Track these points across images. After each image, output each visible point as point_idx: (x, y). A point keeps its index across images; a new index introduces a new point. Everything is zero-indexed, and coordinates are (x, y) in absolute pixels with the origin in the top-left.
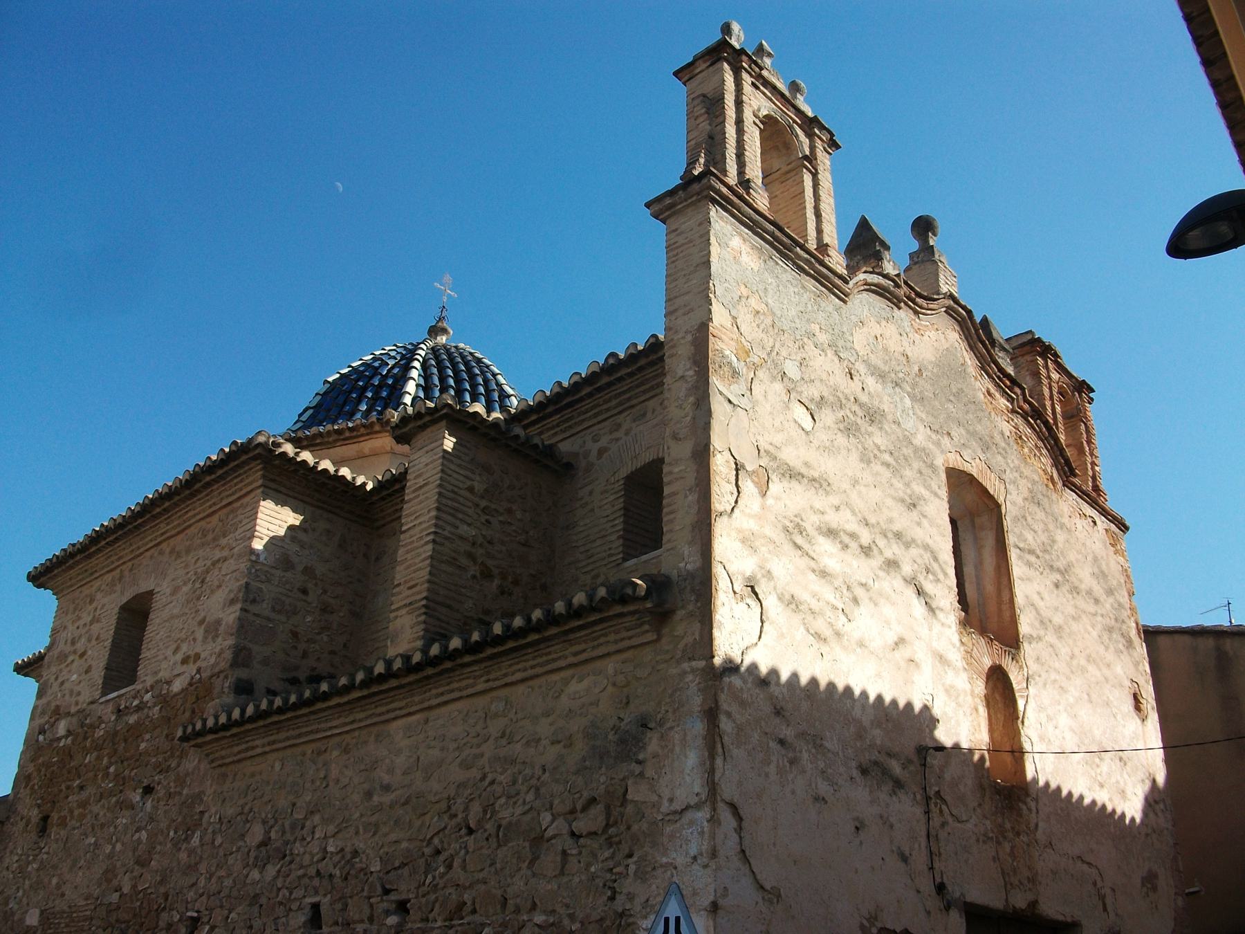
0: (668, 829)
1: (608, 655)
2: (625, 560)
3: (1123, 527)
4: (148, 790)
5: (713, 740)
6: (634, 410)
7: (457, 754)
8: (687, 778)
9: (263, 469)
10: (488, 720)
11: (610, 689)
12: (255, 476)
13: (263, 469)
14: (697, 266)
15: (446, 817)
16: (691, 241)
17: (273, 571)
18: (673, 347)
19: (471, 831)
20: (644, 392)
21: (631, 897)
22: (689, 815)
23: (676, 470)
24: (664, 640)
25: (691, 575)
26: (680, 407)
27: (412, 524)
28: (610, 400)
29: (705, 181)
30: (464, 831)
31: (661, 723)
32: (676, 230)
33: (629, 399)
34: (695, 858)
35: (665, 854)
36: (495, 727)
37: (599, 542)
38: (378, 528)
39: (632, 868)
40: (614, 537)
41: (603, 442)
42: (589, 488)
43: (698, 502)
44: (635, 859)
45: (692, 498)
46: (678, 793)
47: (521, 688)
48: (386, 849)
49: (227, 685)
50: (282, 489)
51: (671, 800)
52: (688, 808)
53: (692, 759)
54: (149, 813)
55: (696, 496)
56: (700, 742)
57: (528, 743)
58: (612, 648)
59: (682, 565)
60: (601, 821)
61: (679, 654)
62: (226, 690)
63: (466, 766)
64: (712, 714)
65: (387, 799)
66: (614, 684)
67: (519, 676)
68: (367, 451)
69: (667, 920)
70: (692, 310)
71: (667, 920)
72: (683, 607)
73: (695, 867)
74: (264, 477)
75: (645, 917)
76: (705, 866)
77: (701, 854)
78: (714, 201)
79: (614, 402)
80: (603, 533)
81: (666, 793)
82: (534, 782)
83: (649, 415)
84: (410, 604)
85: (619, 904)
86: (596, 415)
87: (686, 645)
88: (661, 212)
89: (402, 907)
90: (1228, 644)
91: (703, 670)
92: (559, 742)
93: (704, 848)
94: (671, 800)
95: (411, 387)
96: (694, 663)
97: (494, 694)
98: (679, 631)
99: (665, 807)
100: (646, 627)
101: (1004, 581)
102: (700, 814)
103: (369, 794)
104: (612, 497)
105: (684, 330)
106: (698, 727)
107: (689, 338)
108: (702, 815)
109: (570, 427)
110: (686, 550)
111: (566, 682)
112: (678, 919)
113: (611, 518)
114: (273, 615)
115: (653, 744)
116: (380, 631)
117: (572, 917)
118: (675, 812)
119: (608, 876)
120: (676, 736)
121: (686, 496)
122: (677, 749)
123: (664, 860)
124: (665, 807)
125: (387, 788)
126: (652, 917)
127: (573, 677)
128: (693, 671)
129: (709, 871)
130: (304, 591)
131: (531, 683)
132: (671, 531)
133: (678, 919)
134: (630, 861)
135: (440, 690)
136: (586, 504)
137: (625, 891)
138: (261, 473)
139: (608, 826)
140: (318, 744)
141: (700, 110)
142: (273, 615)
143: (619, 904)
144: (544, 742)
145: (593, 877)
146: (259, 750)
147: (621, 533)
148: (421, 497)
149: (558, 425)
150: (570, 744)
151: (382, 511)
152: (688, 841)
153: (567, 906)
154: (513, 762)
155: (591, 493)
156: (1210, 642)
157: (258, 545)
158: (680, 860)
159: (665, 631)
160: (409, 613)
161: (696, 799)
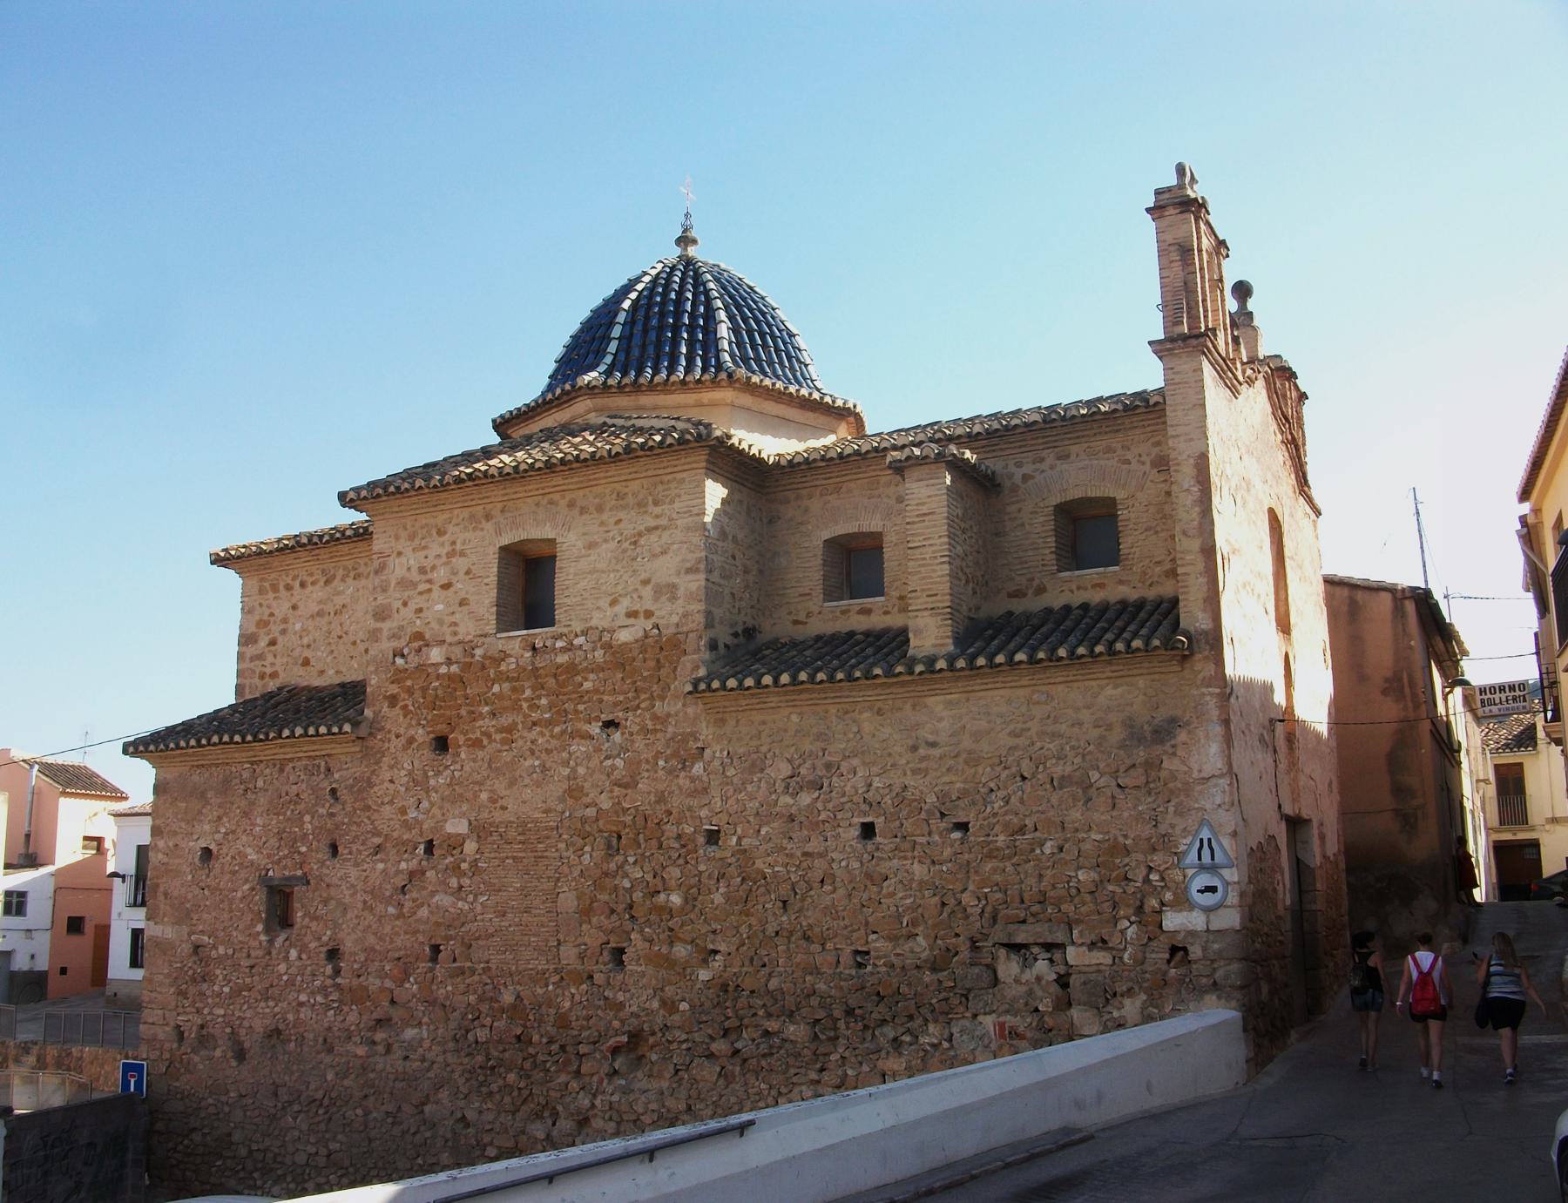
0: (1198, 788)
1: (1142, 674)
2: (1059, 571)
3: (1318, 513)
4: (610, 724)
5: (1228, 740)
6: (1056, 450)
7: (1004, 726)
8: (1211, 759)
9: (709, 454)
10: (1031, 706)
11: (1141, 697)
12: (700, 458)
13: (709, 454)
14: (1195, 405)
15: (998, 769)
16: (1186, 383)
17: (718, 543)
18: (1178, 464)
19: (1024, 778)
20: (1070, 439)
21: (1172, 826)
22: (1214, 781)
23: (1188, 558)
24: (1186, 671)
25: (1205, 633)
26: (1188, 512)
27: (920, 544)
28: (1037, 438)
29: (1202, 340)
30: (1018, 779)
31: (1188, 723)
32: (1172, 369)
33: (1056, 441)
34: (1219, 805)
35: (1197, 801)
36: (1038, 712)
37: (1030, 553)
38: (768, 493)
39: (1171, 809)
40: (1047, 551)
41: (1027, 469)
42: (1018, 506)
43: (1208, 583)
44: (1172, 803)
45: (1203, 580)
46: (1204, 767)
47: (1060, 687)
48: (940, 788)
49: (702, 643)
50: (715, 469)
51: (1200, 771)
52: (1213, 776)
53: (1214, 748)
54: (620, 745)
55: (1206, 580)
56: (1220, 738)
57: (1073, 725)
58: (1145, 671)
59: (1197, 624)
60: (1143, 779)
61: (1199, 682)
62: (703, 648)
63: (1014, 734)
64: (1226, 722)
65: (936, 752)
66: (1145, 694)
67: (1061, 679)
68: (705, 401)
69: (1201, 840)
70: (1191, 440)
71: (1201, 840)
72: (1200, 652)
73: (1220, 810)
74: (708, 461)
75: (1185, 837)
76: (1227, 810)
77: (1224, 803)
78: (1204, 353)
79: (1040, 441)
80: (1036, 546)
81: (1195, 767)
82: (1081, 750)
83: (1073, 457)
84: (932, 609)
85: (1163, 829)
86: (1020, 447)
87: (1204, 678)
88: (1161, 351)
89: (963, 827)
90: (1360, 595)
91: (1218, 694)
92: (1100, 727)
93: (1226, 800)
94: (1200, 771)
95: (724, 330)
96: (1210, 689)
97: (1036, 688)
98: (1198, 667)
99: (1195, 774)
100: (1175, 662)
101: (1282, 584)
102: (1222, 781)
103: (914, 748)
104: (1042, 519)
105: (1187, 453)
106: (1218, 729)
107: (1192, 461)
108: (1224, 782)
109: (994, 451)
110: (1200, 615)
111: (1102, 688)
112: (1209, 840)
113: (1043, 535)
114: (722, 582)
115: (1182, 736)
116: (787, 588)
117: (1126, 836)
118: (1203, 779)
119: (1153, 813)
120: (1200, 733)
121: (1197, 578)
122: (1202, 741)
123: (1197, 806)
124: (1195, 774)
125: (933, 745)
126: (1191, 838)
127: (1108, 685)
128: (1211, 694)
129: (1229, 813)
130: (734, 557)
131: (1070, 685)
132: (1186, 599)
133: (1209, 840)
134: (1169, 804)
135: (985, 681)
136: (1016, 518)
137: (1167, 822)
138: (706, 457)
139: (1147, 782)
140: (847, 706)
141: (1175, 256)
142: (722, 582)
143: (1163, 829)
144: (1086, 725)
145: (1141, 813)
146: (773, 705)
147: (1053, 549)
148: (927, 523)
149: (983, 447)
150: (1109, 727)
151: (777, 481)
152: (1214, 796)
153: (1121, 830)
154: (1061, 736)
155: (1020, 510)
156: (1346, 592)
157: (708, 519)
158: (1208, 806)
159: (1187, 665)
160: (931, 615)
161: (1219, 772)
